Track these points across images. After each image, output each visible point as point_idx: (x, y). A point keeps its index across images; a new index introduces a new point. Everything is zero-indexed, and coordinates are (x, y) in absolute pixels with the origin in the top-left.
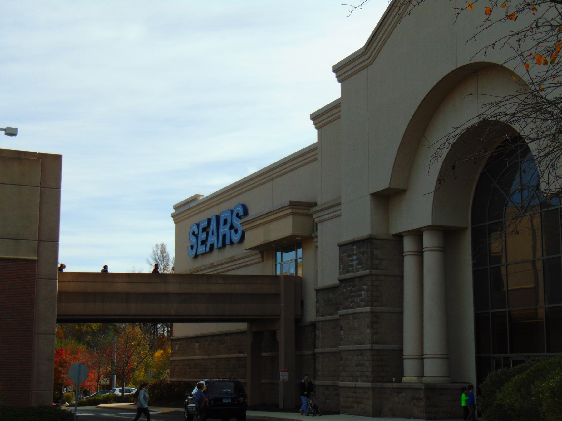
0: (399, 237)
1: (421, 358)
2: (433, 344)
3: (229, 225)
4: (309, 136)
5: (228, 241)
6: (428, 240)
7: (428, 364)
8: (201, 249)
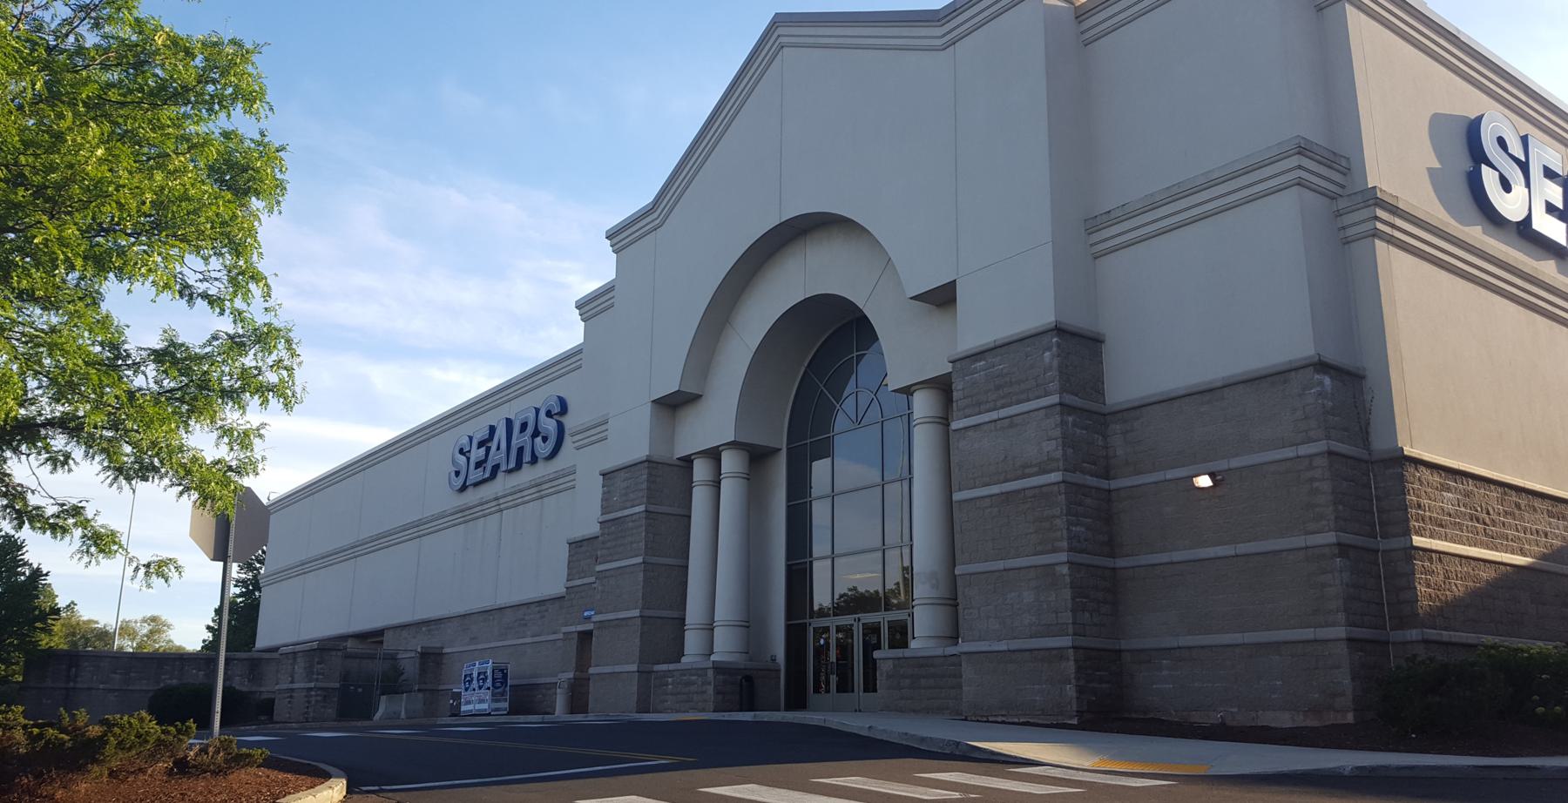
0: (688, 461)
1: (710, 628)
2: (726, 609)
3: (530, 430)
4: (570, 334)
5: (527, 457)
6: (730, 462)
7: (718, 633)
8: (476, 475)
